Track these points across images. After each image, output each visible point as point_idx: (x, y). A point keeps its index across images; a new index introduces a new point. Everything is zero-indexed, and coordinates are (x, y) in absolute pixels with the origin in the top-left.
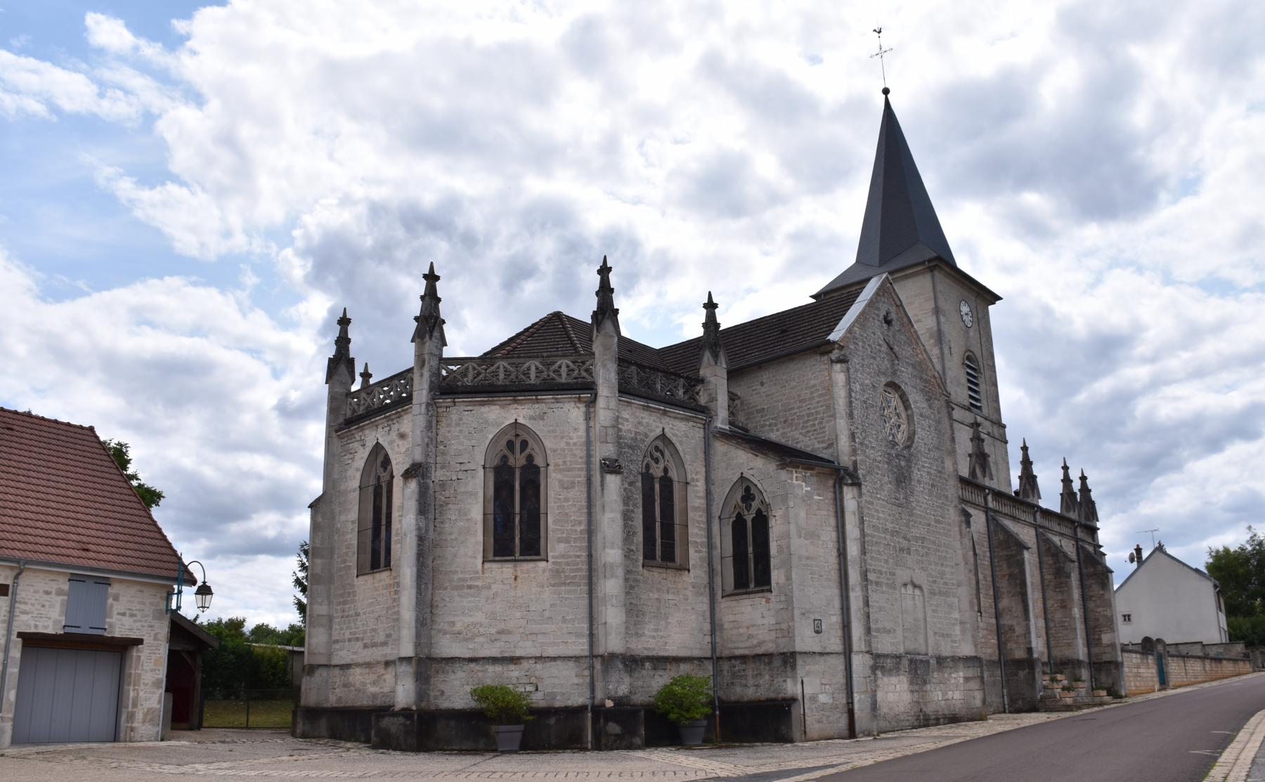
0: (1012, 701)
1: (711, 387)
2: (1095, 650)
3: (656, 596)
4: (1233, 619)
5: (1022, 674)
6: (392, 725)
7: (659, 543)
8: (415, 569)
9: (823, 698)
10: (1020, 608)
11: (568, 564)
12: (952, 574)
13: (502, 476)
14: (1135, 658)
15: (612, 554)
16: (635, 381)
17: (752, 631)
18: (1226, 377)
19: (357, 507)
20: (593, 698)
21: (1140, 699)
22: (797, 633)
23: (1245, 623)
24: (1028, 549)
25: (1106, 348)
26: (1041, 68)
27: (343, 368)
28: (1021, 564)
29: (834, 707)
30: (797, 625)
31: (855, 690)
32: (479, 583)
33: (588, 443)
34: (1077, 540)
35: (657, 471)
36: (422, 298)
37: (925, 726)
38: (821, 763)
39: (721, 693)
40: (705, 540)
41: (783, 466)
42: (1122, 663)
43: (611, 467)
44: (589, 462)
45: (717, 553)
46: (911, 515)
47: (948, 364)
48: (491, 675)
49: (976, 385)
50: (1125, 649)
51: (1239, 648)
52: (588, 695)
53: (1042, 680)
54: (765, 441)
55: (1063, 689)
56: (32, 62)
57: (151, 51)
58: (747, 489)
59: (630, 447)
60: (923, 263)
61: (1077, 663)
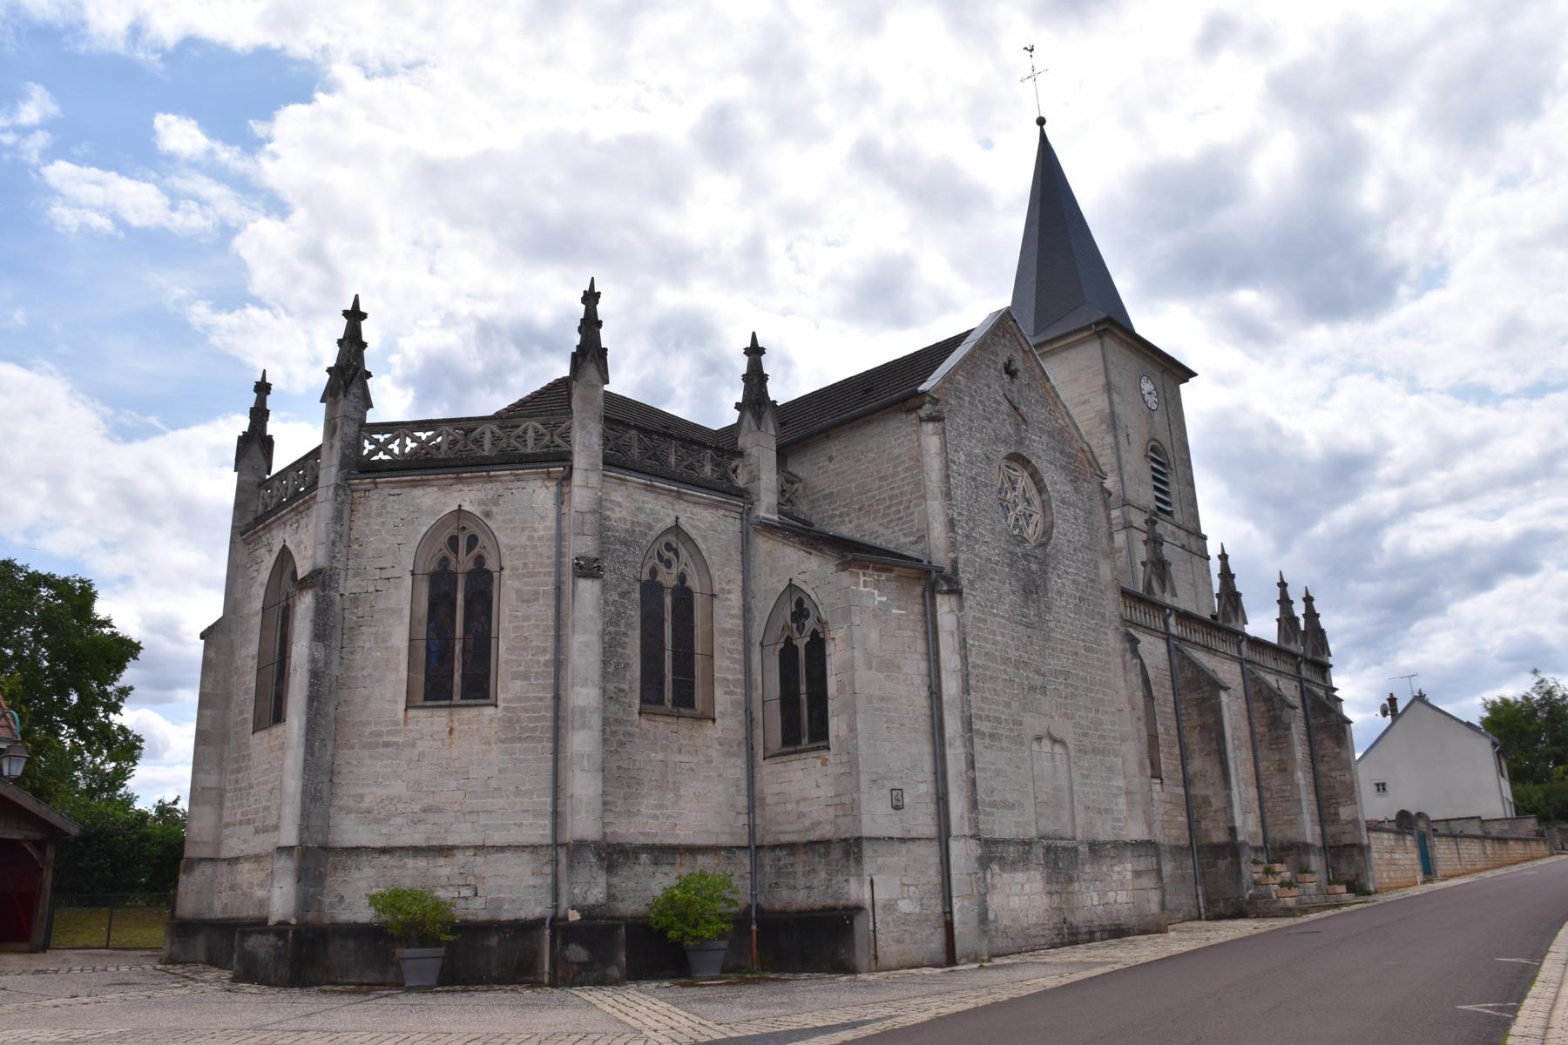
0: (1210, 903)
1: (752, 460)
2: (1331, 829)
3: (660, 756)
4: (1519, 786)
5: (1222, 865)
6: (260, 945)
7: (668, 677)
8: (304, 718)
9: (905, 906)
10: (1217, 772)
11: (525, 710)
12: (1113, 723)
13: (439, 585)
14: (1387, 840)
15: (584, 695)
16: (635, 451)
17: (804, 807)
18: (1493, 500)
19: (257, 637)
20: (556, 907)
21: (1395, 896)
22: (864, 808)
23: (1536, 792)
24: (1226, 689)
25: (1347, 470)
26: (1250, 145)
27: (255, 450)
28: (1217, 711)
29: (922, 920)
30: (863, 797)
31: (954, 893)
32: (399, 739)
33: (560, 537)
34: (1301, 680)
35: (668, 579)
36: (340, 342)
37: (1070, 943)
38: (844, 1019)
39: (761, 899)
40: (740, 677)
41: (844, 566)
42: (1369, 847)
43: (588, 569)
44: (559, 564)
45: (757, 695)
46: (1047, 639)
47: (1125, 456)
48: (409, 874)
49: (1165, 483)
50: (1375, 827)
51: (1530, 824)
52: (549, 902)
53: (1251, 872)
54: (834, 537)
55: (1282, 885)
56: (94, 173)
57: (227, 155)
58: (800, 603)
59: (624, 543)
60: (1088, 327)
61: (1303, 848)
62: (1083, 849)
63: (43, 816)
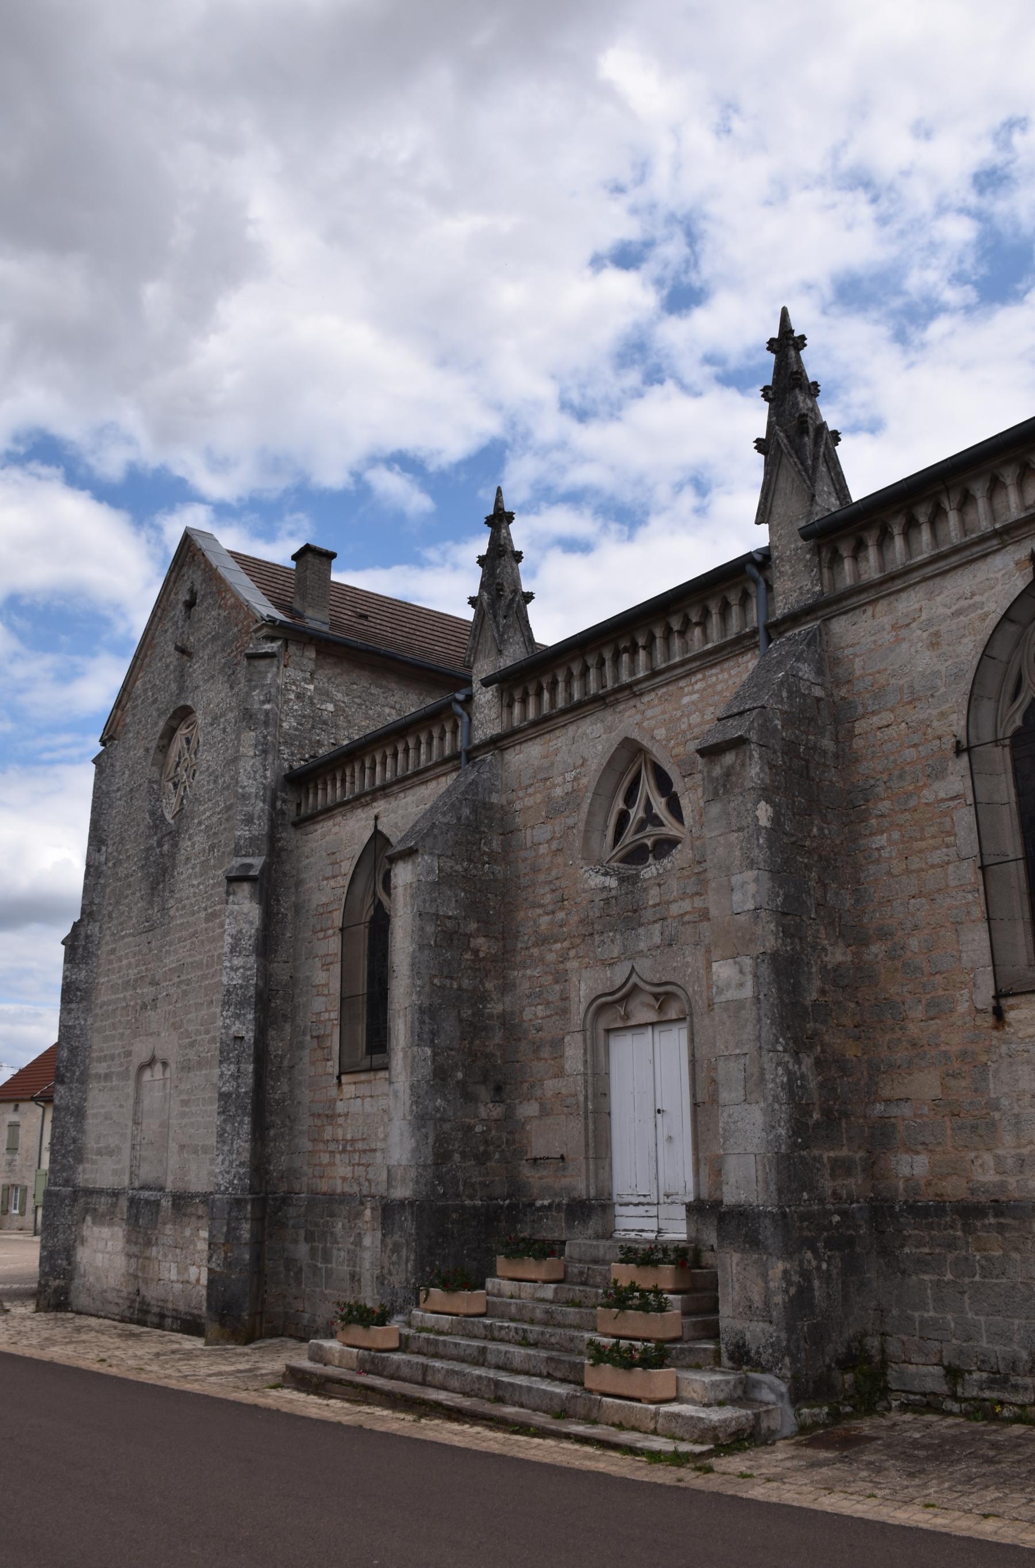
62: (166, 1203)
63: (870, 1516)
